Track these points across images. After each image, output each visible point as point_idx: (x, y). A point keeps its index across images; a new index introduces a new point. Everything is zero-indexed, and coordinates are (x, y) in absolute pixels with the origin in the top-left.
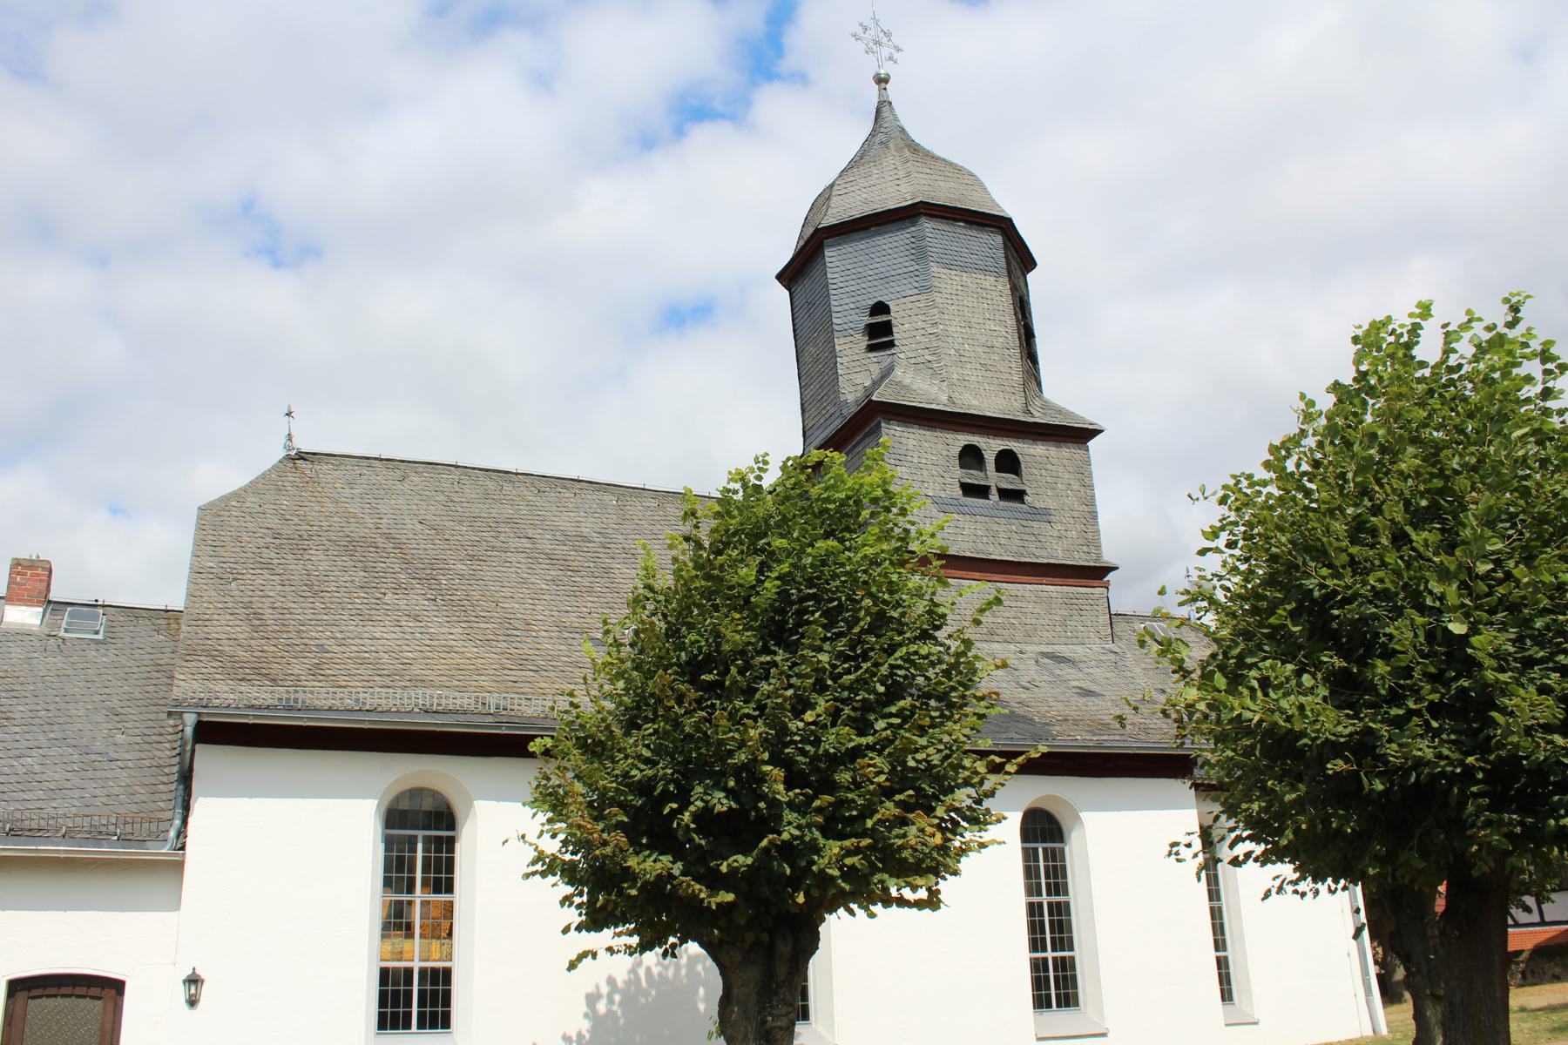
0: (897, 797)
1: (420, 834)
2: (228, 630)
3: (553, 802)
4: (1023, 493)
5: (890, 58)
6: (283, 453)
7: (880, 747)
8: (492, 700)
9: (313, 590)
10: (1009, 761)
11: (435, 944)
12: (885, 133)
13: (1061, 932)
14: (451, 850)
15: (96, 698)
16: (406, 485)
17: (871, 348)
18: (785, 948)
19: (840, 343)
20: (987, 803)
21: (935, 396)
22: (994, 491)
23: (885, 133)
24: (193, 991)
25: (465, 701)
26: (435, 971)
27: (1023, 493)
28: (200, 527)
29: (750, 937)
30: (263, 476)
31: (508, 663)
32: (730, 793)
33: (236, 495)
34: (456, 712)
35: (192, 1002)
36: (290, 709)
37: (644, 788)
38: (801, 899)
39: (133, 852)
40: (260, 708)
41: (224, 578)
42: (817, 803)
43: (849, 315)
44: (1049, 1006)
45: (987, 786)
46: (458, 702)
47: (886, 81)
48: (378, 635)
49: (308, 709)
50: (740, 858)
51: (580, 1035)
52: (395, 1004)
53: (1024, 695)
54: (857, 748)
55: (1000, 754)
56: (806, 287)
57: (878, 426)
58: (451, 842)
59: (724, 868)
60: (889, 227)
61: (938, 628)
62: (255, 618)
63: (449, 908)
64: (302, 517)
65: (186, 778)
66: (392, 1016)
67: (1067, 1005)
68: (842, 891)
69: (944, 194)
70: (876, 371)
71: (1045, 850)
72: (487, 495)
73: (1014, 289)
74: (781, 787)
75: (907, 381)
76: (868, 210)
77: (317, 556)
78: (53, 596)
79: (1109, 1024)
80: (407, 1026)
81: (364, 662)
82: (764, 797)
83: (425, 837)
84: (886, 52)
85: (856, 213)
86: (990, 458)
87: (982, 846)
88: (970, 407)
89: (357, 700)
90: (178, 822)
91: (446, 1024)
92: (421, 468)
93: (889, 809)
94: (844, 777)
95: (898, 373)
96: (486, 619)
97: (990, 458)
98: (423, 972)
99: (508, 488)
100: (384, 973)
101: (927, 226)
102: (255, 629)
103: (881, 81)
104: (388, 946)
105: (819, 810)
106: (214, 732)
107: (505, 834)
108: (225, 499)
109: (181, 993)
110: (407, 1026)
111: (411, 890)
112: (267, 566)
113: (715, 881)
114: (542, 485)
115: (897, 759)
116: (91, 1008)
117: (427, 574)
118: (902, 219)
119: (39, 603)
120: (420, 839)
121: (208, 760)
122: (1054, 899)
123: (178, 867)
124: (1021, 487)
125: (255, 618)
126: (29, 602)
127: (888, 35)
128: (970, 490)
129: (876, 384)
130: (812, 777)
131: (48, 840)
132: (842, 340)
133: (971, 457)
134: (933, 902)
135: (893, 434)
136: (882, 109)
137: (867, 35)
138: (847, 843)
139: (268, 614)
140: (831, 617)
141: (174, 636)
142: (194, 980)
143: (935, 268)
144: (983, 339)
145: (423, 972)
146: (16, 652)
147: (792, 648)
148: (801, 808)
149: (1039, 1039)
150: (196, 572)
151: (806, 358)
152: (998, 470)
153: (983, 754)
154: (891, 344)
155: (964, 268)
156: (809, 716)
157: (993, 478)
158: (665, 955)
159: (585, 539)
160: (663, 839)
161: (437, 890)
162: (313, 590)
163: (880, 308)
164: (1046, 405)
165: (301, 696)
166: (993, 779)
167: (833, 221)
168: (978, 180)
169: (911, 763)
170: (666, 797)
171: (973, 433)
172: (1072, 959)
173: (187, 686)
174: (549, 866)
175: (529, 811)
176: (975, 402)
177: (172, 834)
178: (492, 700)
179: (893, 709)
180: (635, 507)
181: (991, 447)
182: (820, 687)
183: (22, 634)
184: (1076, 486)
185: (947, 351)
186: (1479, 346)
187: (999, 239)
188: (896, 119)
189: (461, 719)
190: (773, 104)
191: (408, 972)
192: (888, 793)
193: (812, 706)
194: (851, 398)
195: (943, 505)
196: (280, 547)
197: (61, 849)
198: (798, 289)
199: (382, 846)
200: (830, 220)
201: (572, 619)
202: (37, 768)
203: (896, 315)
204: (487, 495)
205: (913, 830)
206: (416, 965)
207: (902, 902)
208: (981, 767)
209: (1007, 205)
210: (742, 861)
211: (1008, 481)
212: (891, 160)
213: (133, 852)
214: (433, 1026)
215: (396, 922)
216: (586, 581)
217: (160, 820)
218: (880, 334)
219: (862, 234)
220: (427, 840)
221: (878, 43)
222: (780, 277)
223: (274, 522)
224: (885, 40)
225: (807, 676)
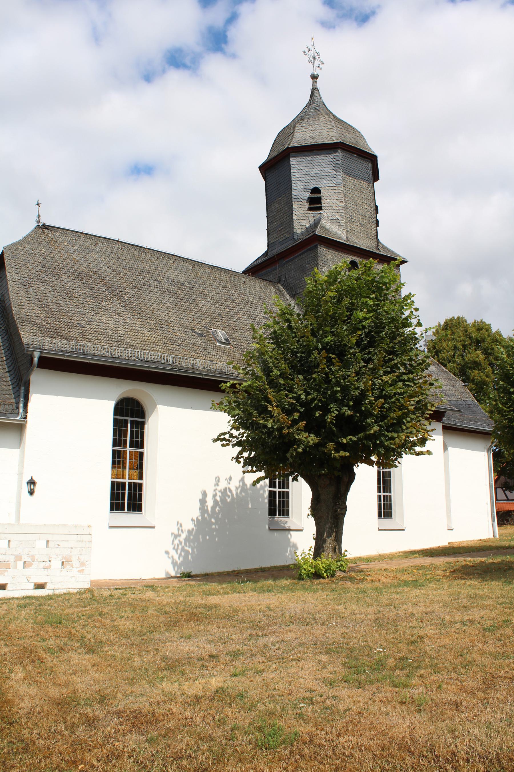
1: (129, 419)
5: (319, 67)
9: (68, 295)
12: (315, 107)
13: (283, 506)
14: (143, 428)
16: (97, 248)
17: (310, 209)
23: (315, 107)
24: (32, 487)
31: (166, 341)
35: (31, 493)
36: (80, 354)
43: (300, 190)
46: (153, 357)
48: (104, 321)
51: (197, 518)
52: (135, 494)
57: (316, 247)
58: (143, 424)
60: (323, 152)
69: (349, 140)
72: (135, 257)
76: (314, 142)
79: (405, 525)
80: (123, 509)
83: (131, 421)
85: (308, 142)
88: (355, 243)
89: (108, 352)
91: (140, 509)
95: (323, 222)
98: (130, 484)
99: (144, 255)
101: (339, 154)
103: (314, 77)
109: (25, 488)
112: (43, 281)
114: (158, 255)
117: (117, 293)
120: (129, 421)
127: (318, 55)
132: (297, 203)
136: (314, 91)
137: (309, 53)
139: (51, 306)
142: (32, 482)
144: (361, 212)
149: (379, 530)
154: (320, 209)
155: (355, 177)
159: (182, 284)
162: (68, 295)
167: (296, 145)
171: (355, 256)
176: (357, 241)
180: (201, 272)
188: (321, 98)
190: (214, 65)
194: (299, 231)
200: (295, 143)
201: (185, 322)
203: (324, 194)
206: (127, 481)
209: (375, 149)
214: (134, 510)
215: (117, 459)
216: (187, 305)
218: (315, 202)
219: (309, 153)
220: (132, 422)
223: (40, 259)
224: (317, 57)
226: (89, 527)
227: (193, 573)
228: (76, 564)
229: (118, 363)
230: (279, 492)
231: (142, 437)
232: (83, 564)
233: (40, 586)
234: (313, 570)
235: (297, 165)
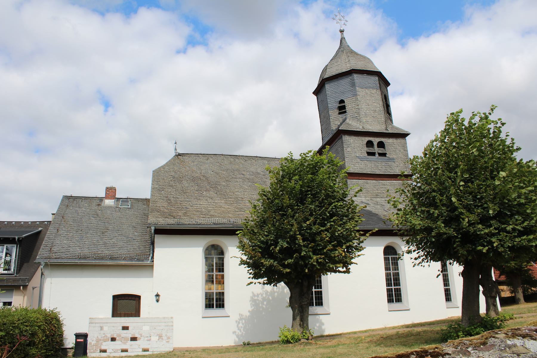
0: (332, 243)
2: (162, 204)
3: (242, 247)
4: (386, 154)
6: (175, 154)
7: (327, 230)
8: (232, 220)
9: (184, 192)
10: (367, 233)
11: (220, 286)
12: (343, 48)
14: (223, 261)
15: (130, 223)
17: (340, 113)
18: (305, 284)
19: (331, 112)
20: (361, 245)
22: (377, 154)
23: (343, 48)
25: (225, 221)
27: (386, 154)
28: (153, 177)
29: (296, 281)
30: (170, 161)
32: (287, 243)
33: (163, 167)
34: (222, 224)
35: (158, 301)
36: (178, 225)
37: (266, 243)
38: (307, 271)
39: (140, 263)
40: (170, 225)
41: (160, 190)
42: (310, 246)
44: (393, 302)
45: (361, 240)
47: (343, 31)
49: (183, 225)
50: (290, 260)
53: (385, 213)
54: (322, 231)
55: (362, 231)
56: (321, 96)
57: (342, 137)
59: (286, 263)
60: (344, 77)
61: (345, 197)
62: (169, 201)
63: (223, 276)
64: (183, 170)
65: (153, 243)
66: (209, 305)
67: (399, 302)
68: (317, 269)
69: (360, 66)
71: (391, 258)
73: (382, 93)
74: (301, 241)
75: (350, 123)
76: (337, 72)
77: (185, 182)
78: (117, 197)
79: (331, 311)
80: (213, 307)
81: (198, 211)
82: (297, 244)
84: (343, 22)
85: (334, 74)
86: (375, 144)
87: (359, 256)
90: (151, 255)
91: (401, 301)
92: (212, 156)
93: (330, 247)
94: (318, 238)
95: (347, 120)
96: (231, 198)
97: (375, 144)
98: (216, 293)
99: (237, 160)
100: (206, 293)
101: (355, 76)
103: (342, 31)
104: (207, 286)
105: (311, 247)
106: (160, 231)
107: (234, 254)
108: (160, 168)
109: (154, 299)
110: (213, 307)
111: (213, 271)
113: (285, 266)
115: (333, 234)
116: (133, 302)
118: (347, 75)
119: (114, 199)
121: (158, 239)
123: (152, 266)
124: (385, 152)
125: (169, 201)
126: (111, 199)
128: (369, 154)
129: (341, 124)
130: (310, 238)
131: (120, 260)
133: (370, 144)
134: (348, 271)
135: (346, 139)
136: (342, 40)
138: (318, 256)
139: (172, 199)
140: (314, 196)
141: (148, 206)
142: (157, 295)
143: (357, 89)
145: (216, 293)
146: (109, 212)
147: (303, 204)
148: (306, 246)
150: (153, 189)
151: (322, 117)
152: (378, 147)
153: (358, 231)
154: (345, 112)
155: (366, 88)
156: (308, 223)
157: (376, 149)
158: (274, 286)
159: (258, 173)
160: (271, 256)
161: (220, 272)
162: (184, 192)
163: (342, 101)
164: (394, 127)
165: (181, 221)
166: (362, 238)
168: (370, 60)
169: (337, 234)
170: (271, 245)
172: (400, 289)
173: (152, 219)
174: (243, 262)
175: (238, 250)
176: (370, 128)
177: (150, 258)
178: (232, 220)
179: (332, 220)
181: (376, 140)
182: (311, 215)
183: (110, 207)
184: (402, 151)
185: (364, 114)
186: (481, 118)
187: (377, 78)
188: (346, 43)
189: (224, 226)
191: (213, 293)
192: (330, 242)
193: (308, 220)
195: (362, 159)
196: (174, 181)
197: (123, 262)
198: (319, 96)
199: (204, 260)
202: (116, 242)
203: (346, 103)
204: (231, 163)
205: (337, 252)
206: (215, 291)
207: (340, 272)
208: (357, 235)
209: (380, 67)
210: (290, 261)
211: (381, 150)
212: (344, 56)
213: (140, 263)
214: (220, 307)
215: (210, 280)
217: (147, 255)
218: (342, 109)
219: (336, 80)
221: (340, 20)
222: (314, 93)
223: (173, 174)
224: (342, 19)
225: (307, 212)
226: (172, 318)
227: (251, 343)
228: (165, 338)
229: (199, 227)
230: (395, 289)
232: (168, 338)
233: (145, 350)
234: (286, 339)
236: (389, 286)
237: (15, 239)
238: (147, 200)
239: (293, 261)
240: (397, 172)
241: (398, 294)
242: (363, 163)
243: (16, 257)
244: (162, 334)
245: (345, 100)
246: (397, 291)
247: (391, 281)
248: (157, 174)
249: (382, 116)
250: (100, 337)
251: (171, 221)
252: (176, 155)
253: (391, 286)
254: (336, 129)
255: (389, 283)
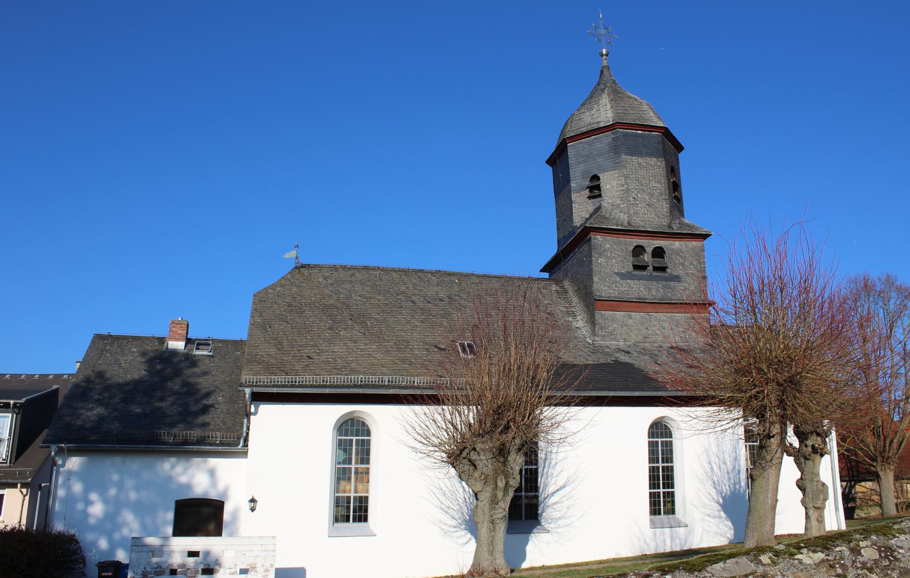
6: (294, 266)
17: (589, 198)
21: (621, 218)
26: (361, 497)
35: (253, 509)
43: (578, 181)
63: (367, 472)
70: (591, 209)
80: (660, 514)
86: (649, 250)
91: (366, 520)
98: (355, 498)
102: (279, 349)
109: (248, 506)
111: (350, 463)
122: (655, 465)
142: (253, 501)
150: (252, 324)
154: (600, 196)
161: (362, 463)
181: (650, 244)
191: (349, 498)
195: (622, 276)
206: (352, 495)
211: (658, 262)
215: (341, 475)
218: (595, 190)
222: (548, 162)
226: (274, 537)
231: (672, 453)
235: (572, 148)
236: (654, 488)
237: (9, 404)
238: (238, 344)
239: (644, 102)
240: (685, 298)
241: (668, 475)
242: (624, 282)
243: (10, 435)
244: (255, 564)
245: (601, 176)
246: (667, 446)
247: (659, 480)
248: (261, 300)
249: (664, 207)
250: (149, 569)
251: (280, 379)
252: (296, 268)
253: (659, 488)
254: (582, 225)
255: (654, 484)
